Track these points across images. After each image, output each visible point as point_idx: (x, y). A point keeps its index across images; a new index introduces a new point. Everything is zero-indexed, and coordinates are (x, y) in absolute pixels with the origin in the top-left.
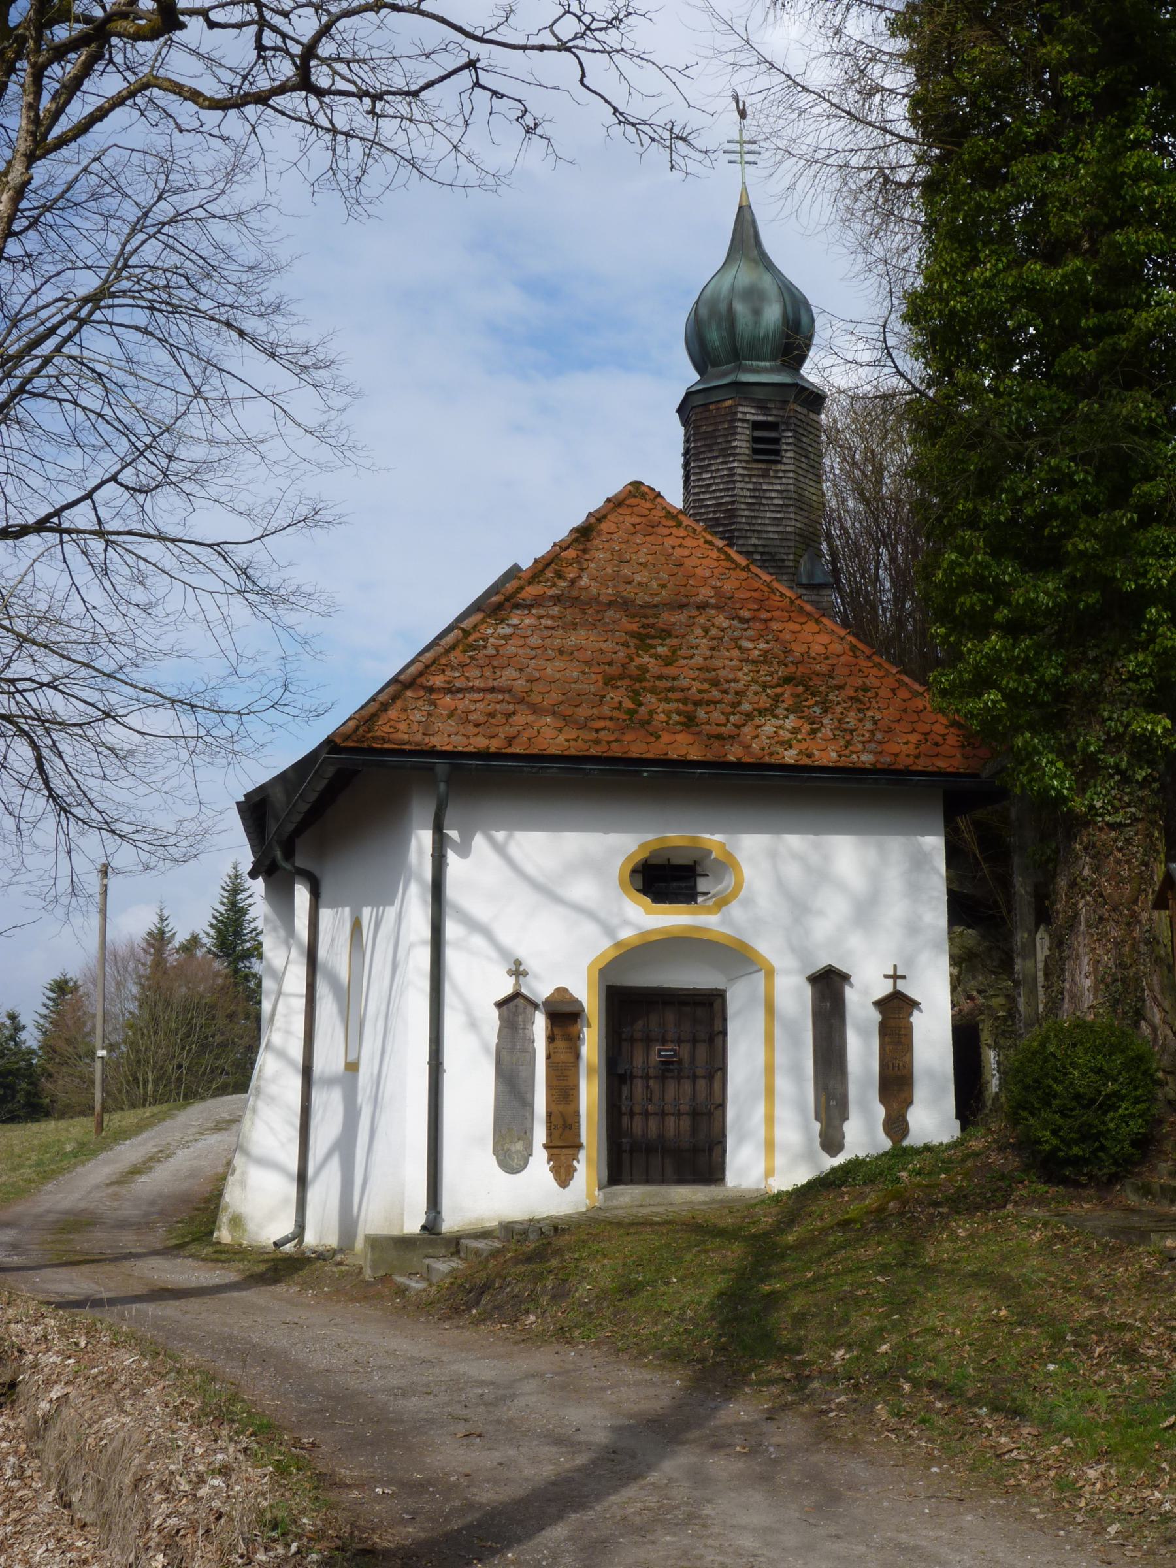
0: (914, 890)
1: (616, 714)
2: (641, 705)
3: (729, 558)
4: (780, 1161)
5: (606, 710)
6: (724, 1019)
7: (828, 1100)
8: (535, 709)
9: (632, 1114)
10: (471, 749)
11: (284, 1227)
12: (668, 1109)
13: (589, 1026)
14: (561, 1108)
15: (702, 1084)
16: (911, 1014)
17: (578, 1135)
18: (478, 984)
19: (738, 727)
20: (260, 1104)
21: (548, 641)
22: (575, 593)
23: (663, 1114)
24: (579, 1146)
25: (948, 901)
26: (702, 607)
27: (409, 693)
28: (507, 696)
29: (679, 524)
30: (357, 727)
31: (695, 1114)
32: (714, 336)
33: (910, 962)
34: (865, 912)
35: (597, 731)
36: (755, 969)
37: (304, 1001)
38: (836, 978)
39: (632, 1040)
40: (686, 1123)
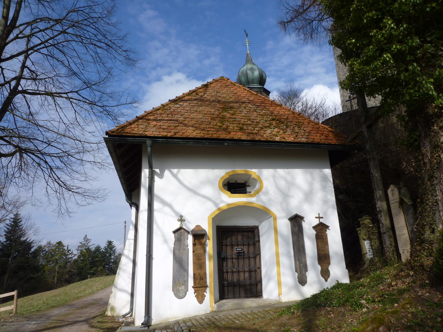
0: (324, 188)
1: (215, 127)
2: (224, 125)
3: (251, 92)
4: (284, 290)
5: (212, 126)
6: (259, 237)
7: (300, 264)
8: (186, 125)
9: (227, 272)
10: (161, 136)
11: (126, 310)
12: (240, 270)
13: (209, 239)
14: (199, 271)
15: (252, 260)
16: (326, 231)
17: (206, 282)
18: (166, 224)
19: (258, 131)
20: (121, 272)
21: (192, 109)
22: (202, 98)
23: (239, 272)
24: (206, 287)
25: (335, 191)
26: (243, 103)
27: (140, 121)
28: (176, 122)
29: (235, 85)
30: (118, 129)
31: (250, 271)
32: (243, 79)
33: (325, 214)
34: (308, 196)
35: (208, 131)
36: (270, 216)
37: (133, 241)
38: (299, 219)
39: (226, 245)
40: (247, 275)
